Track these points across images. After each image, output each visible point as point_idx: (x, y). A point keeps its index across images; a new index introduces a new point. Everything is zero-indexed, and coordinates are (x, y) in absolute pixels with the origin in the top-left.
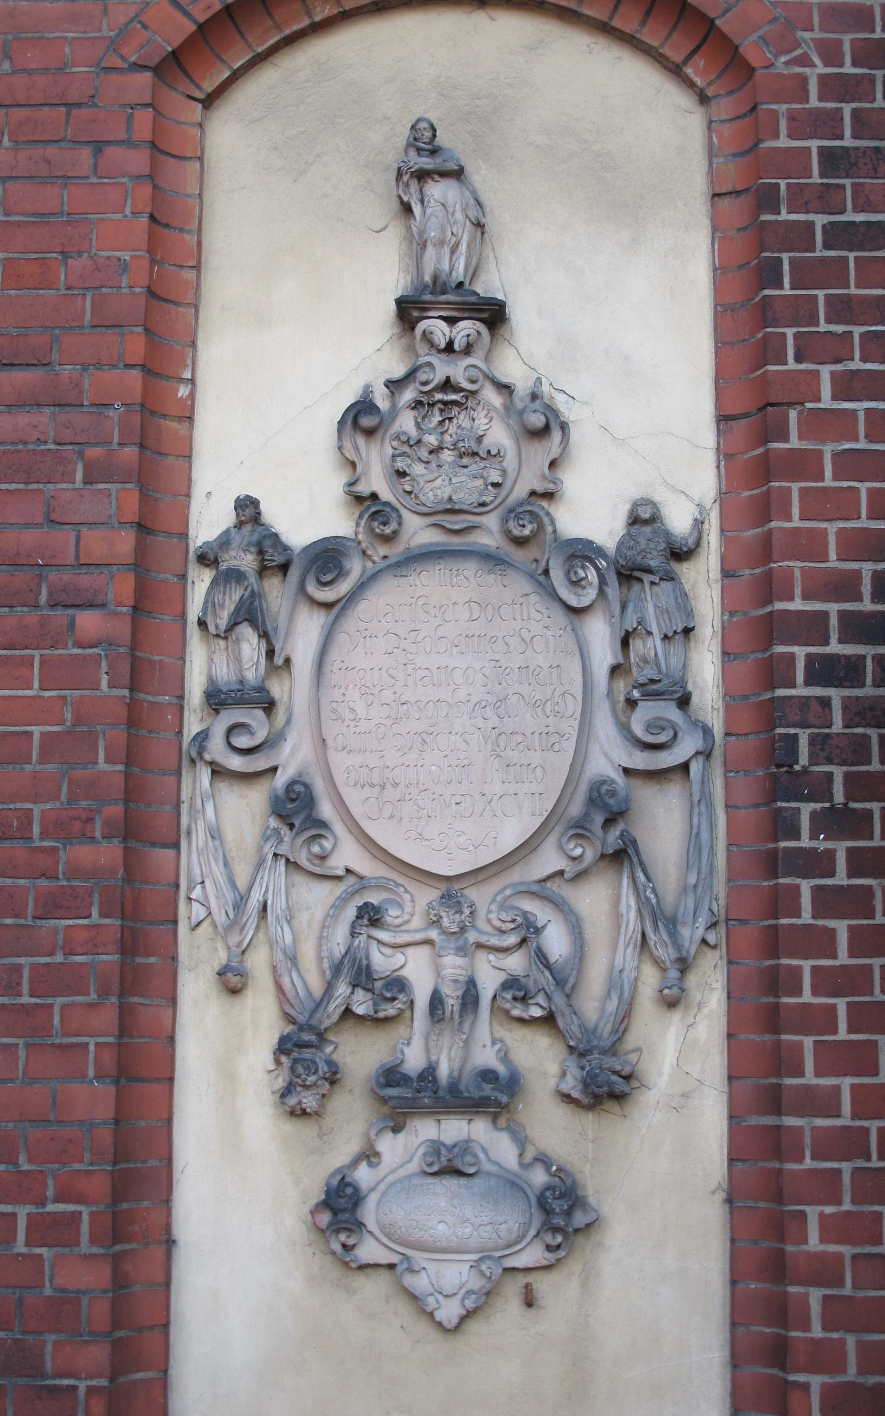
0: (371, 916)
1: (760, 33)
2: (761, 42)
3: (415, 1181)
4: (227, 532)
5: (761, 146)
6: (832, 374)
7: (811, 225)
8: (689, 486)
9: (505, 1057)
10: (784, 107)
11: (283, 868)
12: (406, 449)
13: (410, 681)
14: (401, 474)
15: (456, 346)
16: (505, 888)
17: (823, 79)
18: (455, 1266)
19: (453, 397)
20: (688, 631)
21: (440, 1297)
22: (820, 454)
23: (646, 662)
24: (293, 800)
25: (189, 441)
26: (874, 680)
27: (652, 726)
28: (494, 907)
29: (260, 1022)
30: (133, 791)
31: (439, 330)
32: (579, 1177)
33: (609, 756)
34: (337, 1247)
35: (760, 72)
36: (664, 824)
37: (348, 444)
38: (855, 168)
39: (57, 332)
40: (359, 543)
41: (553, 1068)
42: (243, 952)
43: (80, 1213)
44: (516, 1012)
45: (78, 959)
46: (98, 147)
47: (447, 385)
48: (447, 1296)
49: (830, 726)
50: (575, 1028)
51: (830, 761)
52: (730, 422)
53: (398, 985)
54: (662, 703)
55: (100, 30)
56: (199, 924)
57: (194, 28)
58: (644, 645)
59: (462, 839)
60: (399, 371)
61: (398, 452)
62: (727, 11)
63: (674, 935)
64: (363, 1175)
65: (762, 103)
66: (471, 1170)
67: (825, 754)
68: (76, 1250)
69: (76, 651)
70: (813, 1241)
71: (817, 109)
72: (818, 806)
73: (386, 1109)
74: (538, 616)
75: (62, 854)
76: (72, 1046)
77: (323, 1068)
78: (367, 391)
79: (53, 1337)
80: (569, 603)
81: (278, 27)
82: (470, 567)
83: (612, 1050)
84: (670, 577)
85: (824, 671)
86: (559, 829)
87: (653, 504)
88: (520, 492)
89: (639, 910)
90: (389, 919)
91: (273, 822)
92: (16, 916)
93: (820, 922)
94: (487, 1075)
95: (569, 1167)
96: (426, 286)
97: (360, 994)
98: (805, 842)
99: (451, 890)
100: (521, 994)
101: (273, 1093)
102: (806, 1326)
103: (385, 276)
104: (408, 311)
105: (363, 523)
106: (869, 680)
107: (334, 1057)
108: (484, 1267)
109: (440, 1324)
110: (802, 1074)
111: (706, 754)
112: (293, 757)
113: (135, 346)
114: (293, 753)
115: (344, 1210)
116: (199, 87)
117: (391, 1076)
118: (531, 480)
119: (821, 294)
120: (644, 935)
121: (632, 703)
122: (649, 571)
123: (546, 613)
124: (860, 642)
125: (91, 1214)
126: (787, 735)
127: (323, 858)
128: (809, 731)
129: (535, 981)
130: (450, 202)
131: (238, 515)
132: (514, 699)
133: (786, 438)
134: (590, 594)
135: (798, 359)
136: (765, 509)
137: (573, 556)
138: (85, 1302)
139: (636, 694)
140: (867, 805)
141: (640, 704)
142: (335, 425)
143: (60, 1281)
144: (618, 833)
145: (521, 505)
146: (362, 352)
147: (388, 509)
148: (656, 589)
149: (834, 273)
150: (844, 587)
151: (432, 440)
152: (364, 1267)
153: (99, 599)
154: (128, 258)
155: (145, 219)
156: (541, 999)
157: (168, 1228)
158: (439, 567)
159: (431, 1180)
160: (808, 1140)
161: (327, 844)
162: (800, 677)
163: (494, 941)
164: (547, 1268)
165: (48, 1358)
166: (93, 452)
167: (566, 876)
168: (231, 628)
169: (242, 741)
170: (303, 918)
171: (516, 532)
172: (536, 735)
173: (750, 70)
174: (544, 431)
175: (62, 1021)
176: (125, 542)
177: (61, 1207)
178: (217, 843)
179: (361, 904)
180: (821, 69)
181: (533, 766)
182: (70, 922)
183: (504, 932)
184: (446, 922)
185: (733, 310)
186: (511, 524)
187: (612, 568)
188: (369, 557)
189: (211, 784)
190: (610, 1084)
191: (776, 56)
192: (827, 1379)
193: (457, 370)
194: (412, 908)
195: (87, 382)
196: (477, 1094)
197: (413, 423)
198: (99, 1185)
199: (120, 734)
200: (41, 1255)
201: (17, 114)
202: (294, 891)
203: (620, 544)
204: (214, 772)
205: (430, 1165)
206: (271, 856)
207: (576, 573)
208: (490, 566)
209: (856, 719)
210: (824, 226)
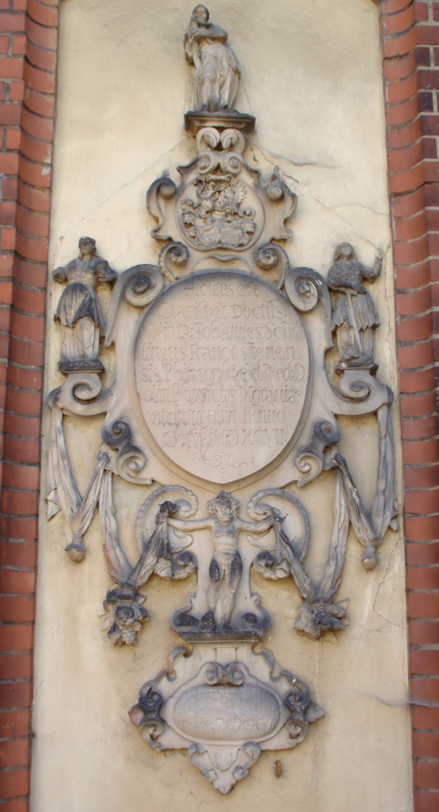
3: (200, 690)
4: (74, 262)
8: (373, 234)
9: (259, 606)
11: (110, 480)
12: (191, 210)
14: (188, 225)
20: (375, 327)
23: (349, 345)
27: (354, 386)
28: (251, 505)
29: (95, 580)
33: (326, 406)
36: (363, 449)
37: (153, 206)
41: (292, 613)
42: (83, 535)
47: (218, 169)
48: (222, 771)
52: (398, 198)
53: (188, 557)
54: (361, 372)
64: (164, 687)
74: (279, 315)
82: (234, 286)
83: (331, 600)
86: (293, 453)
91: (105, 448)
94: (249, 617)
100: (271, 562)
103: (180, 104)
104: (192, 122)
105: (164, 255)
112: (118, 406)
113: (14, 137)
118: (272, 229)
120: (350, 523)
127: (138, 471)
129: (281, 554)
139: (344, 365)
142: (145, 194)
146: (161, 147)
147: (180, 246)
148: (354, 299)
151: (208, 204)
152: (165, 751)
154: (9, 82)
156: (284, 565)
157: (30, 726)
158: (213, 283)
161: (140, 463)
163: (252, 527)
164: (290, 749)
167: (299, 484)
169: (83, 394)
170: (123, 513)
172: (279, 392)
174: (281, 199)
178: (66, 462)
185: (398, 128)
188: (167, 278)
193: (224, 160)
194: (197, 507)
202: (117, 495)
204: (64, 416)
205: (212, 679)
206: (102, 471)
207: (303, 288)
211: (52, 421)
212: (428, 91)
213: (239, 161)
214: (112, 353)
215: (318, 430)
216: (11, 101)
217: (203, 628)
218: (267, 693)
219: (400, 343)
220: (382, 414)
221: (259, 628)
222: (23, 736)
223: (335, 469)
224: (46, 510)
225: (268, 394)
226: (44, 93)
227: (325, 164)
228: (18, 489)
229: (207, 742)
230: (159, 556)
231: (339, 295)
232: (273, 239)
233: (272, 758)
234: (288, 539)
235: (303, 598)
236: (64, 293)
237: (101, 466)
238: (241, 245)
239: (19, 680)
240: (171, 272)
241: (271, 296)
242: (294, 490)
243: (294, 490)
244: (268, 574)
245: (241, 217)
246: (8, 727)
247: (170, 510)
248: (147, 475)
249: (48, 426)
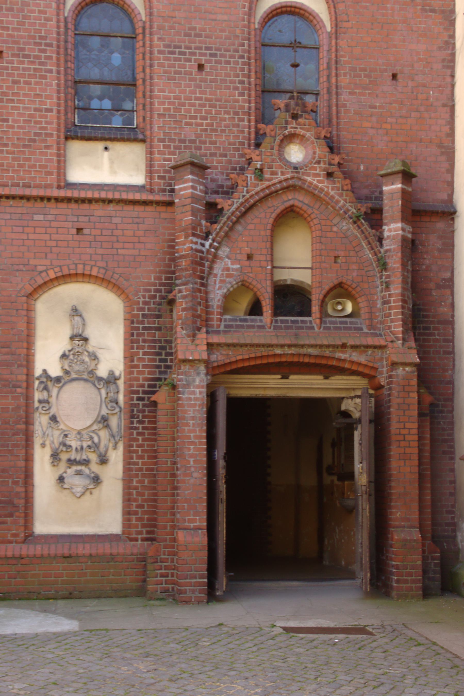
9: (87, 457)
17: (143, 301)
20: (118, 392)
27: (112, 407)
29: (48, 452)
30: (27, 417)
33: (104, 411)
36: (114, 422)
46: (17, 310)
47: (78, 352)
53: (70, 446)
60: (70, 348)
63: (114, 439)
64: (65, 475)
70: (135, 484)
83: (105, 456)
84: (115, 383)
85: (139, 399)
91: (50, 421)
94: (85, 460)
98: (135, 425)
103: (67, 332)
104: (72, 338)
112: (53, 411)
113: (25, 345)
118: (92, 367)
134: (102, 386)
150: (143, 386)
151: (75, 360)
152: (65, 489)
169: (44, 409)
176: (24, 377)
194: (73, 435)
198: (23, 476)
199: (24, 408)
211: (36, 415)
218: (88, 476)
219: (125, 396)
223: (106, 426)
224: (36, 435)
227: (107, 349)
233: (89, 490)
237: (49, 425)
242: (97, 431)
244: (89, 450)
247: (66, 436)
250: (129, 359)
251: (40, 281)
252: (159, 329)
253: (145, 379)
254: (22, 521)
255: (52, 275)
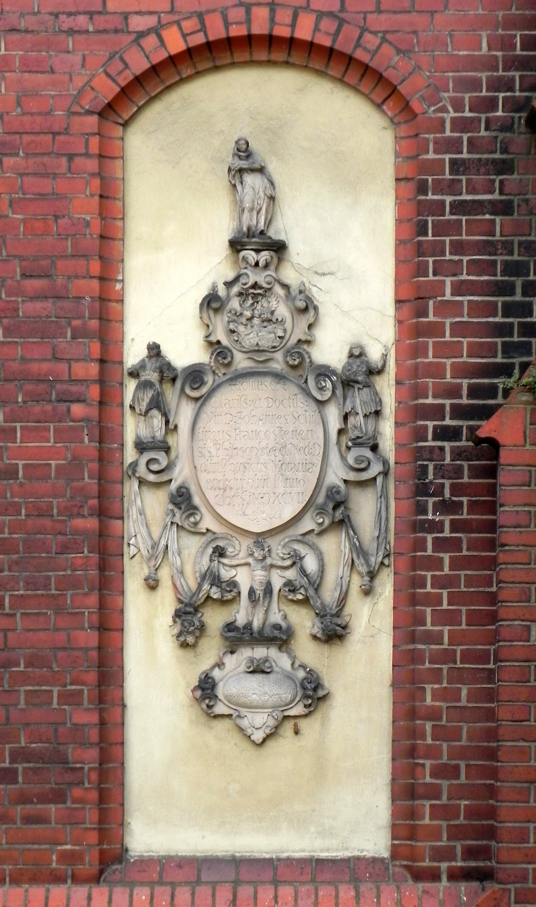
0: (220, 553)
1: (421, 93)
2: (421, 99)
3: (241, 675)
4: (143, 361)
5: (420, 157)
6: (452, 282)
7: (443, 202)
8: (380, 337)
10: (432, 136)
11: (176, 529)
12: (235, 318)
13: (238, 437)
14: (232, 332)
15: (260, 264)
16: (285, 538)
18: (261, 715)
19: (259, 291)
21: (253, 729)
22: (444, 324)
23: (356, 427)
24: (180, 496)
25: (122, 312)
26: (466, 438)
27: (358, 460)
28: (280, 547)
29: (166, 603)
30: (102, 494)
31: (251, 256)
32: (320, 674)
33: (337, 474)
34: (204, 706)
35: (420, 117)
36: (365, 509)
37: (205, 316)
38: (468, 170)
39: (54, 258)
40: (212, 367)
41: (309, 624)
42: (157, 569)
43: (83, 690)
44: (290, 597)
45: (78, 573)
46: (71, 157)
47: (255, 286)
48: (257, 729)
49: (444, 460)
50: (318, 604)
51: (443, 477)
52: (402, 304)
53: (233, 584)
54: (363, 449)
55: (69, 90)
56: (134, 556)
57: (118, 89)
58: (355, 419)
59: (264, 515)
60: (230, 275)
61: (230, 320)
62: (403, 81)
63: (367, 561)
64: (217, 674)
65: (420, 134)
66: (269, 670)
67: (441, 474)
68: (82, 706)
69: (72, 424)
71: (449, 137)
72: (437, 499)
73: (227, 643)
74: (302, 405)
75: (69, 524)
76: (77, 613)
77: (197, 623)
78: (214, 288)
79: (72, 746)
80: (318, 398)
81: (162, 82)
82: (268, 381)
83: (338, 615)
85: (443, 433)
86: (312, 509)
87: (361, 347)
88: (293, 340)
89: (351, 549)
90: (228, 553)
91: (171, 507)
92: (47, 553)
93: (436, 554)
95: (315, 670)
96: (244, 234)
97: (214, 589)
99: (260, 539)
100: (293, 588)
101: (172, 636)
102: (424, 738)
103: (224, 228)
104: (236, 245)
105: (213, 357)
106: (464, 438)
107: (202, 619)
108: (274, 714)
109: (253, 742)
110: (425, 624)
111: (385, 473)
112: (180, 474)
113: (95, 267)
114: (180, 472)
115: (208, 689)
116: (120, 117)
117: (230, 627)
118: (299, 333)
119: (447, 239)
120: (353, 560)
121: (349, 448)
122: (357, 382)
123: (306, 404)
124: (460, 419)
125: (88, 690)
126: (423, 465)
127: (196, 524)
128: (433, 463)
129: (300, 583)
130: (257, 186)
131: (149, 352)
132: (289, 446)
133: (427, 316)
135: (435, 274)
136: (418, 351)
137: (319, 375)
138: (86, 730)
139: (350, 444)
140: (461, 499)
141: (352, 449)
142: (198, 305)
143: (75, 721)
144: (341, 511)
145: (293, 348)
146: (212, 266)
147: (226, 351)
148: (361, 391)
149: (456, 227)
150: (453, 392)
151: (248, 314)
153: (82, 398)
154: (89, 219)
155: (97, 198)
156: (302, 591)
157: (122, 699)
158: (252, 380)
159: (249, 675)
160: (427, 655)
161: (198, 518)
162: (430, 437)
163: (280, 563)
164: (306, 716)
165: (70, 755)
166: (76, 322)
167: (315, 532)
168: (147, 412)
169: (155, 467)
170: (185, 553)
171: (291, 363)
172: (301, 464)
173: (415, 115)
174: (305, 310)
175: (71, 601)
176: (94, 369)
177: (73, 687)
178: (143, 517)
179: (214, 546)
180: (452, 114)
181: (298, 480)
182: (74, 555)
183: (285, 559)
184: (256, 555)
185: (404, 243)
186: (288, 358)
187: (340, 380)
188: (217, 374)
189: (139, 487)
190: (335, 630)
191: (429, 107)
192: (434, 762)
193: (261, 278)
194: (239, 550)
195: (70, 285)
196: (271, 636)
197: (238, 303)
199: (95, 465)
200: (65, 709)
201: (27, 138)
202: (181, 540)
203: (344, 368)
204: (140, 482)
205: (249, 668)
206: (170, 523)
207: (321, 384)
208: (277, 380)
209: (457, 457)
210: (450, 203)
211: (131, 487)
212: (425, 218)
213: (273, 277)
214: (175, 433)
215: (330, 493)
216: (91, 235)
217: (243, 634)
218: (289, 677)
220: (379, 480)
221: (283, 633)
222: (118, 705)
224: (129, 551)
225: (293, 466)
226: (115, 219)
228: (109, 536)
229: (247, 710)
230: (212, 585)
231: (351, 388)
232: (299, 341)
234: (305, 572)
235: (317, 613)
236: (137, 387)
238: (274, 347)
239: (115, 668)
240: (220, 370)
241: (296, 390)
243: (311, 538)
245: (274, 323)
246: (108, 698)
248: (202, 527)
249: (128, 489)
250: (413, 301)
251: (139, 64)
252: (504, 208)
253: (461, 371)
254: (90, 815)
255: (176, 44)
